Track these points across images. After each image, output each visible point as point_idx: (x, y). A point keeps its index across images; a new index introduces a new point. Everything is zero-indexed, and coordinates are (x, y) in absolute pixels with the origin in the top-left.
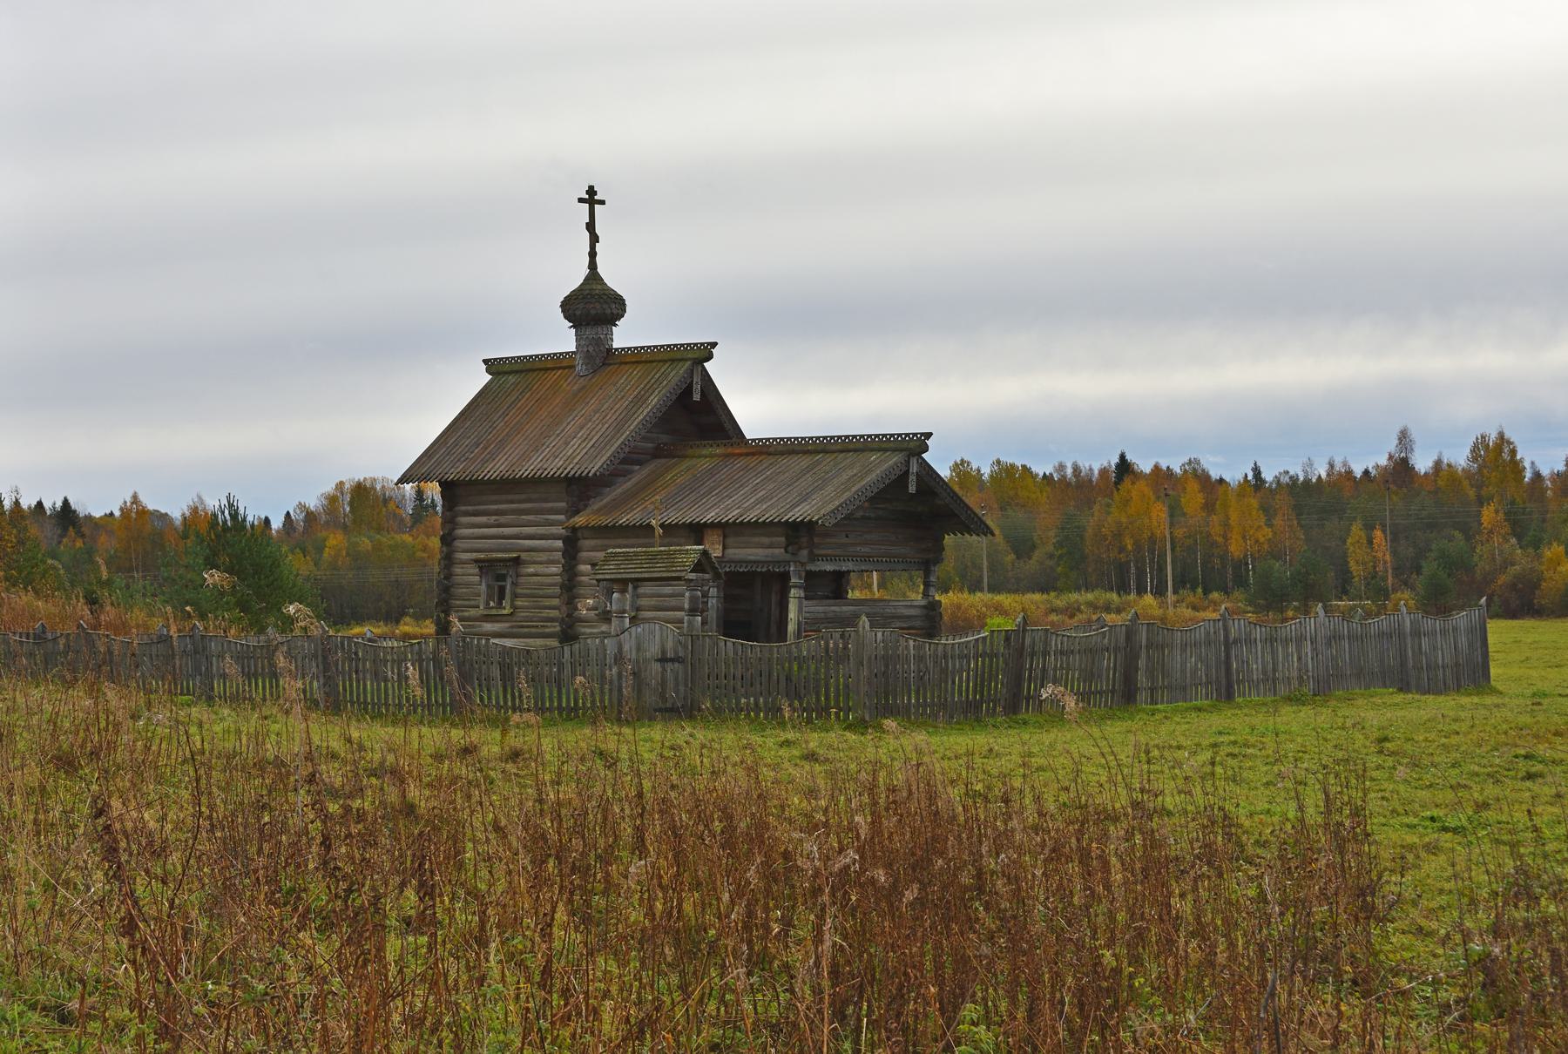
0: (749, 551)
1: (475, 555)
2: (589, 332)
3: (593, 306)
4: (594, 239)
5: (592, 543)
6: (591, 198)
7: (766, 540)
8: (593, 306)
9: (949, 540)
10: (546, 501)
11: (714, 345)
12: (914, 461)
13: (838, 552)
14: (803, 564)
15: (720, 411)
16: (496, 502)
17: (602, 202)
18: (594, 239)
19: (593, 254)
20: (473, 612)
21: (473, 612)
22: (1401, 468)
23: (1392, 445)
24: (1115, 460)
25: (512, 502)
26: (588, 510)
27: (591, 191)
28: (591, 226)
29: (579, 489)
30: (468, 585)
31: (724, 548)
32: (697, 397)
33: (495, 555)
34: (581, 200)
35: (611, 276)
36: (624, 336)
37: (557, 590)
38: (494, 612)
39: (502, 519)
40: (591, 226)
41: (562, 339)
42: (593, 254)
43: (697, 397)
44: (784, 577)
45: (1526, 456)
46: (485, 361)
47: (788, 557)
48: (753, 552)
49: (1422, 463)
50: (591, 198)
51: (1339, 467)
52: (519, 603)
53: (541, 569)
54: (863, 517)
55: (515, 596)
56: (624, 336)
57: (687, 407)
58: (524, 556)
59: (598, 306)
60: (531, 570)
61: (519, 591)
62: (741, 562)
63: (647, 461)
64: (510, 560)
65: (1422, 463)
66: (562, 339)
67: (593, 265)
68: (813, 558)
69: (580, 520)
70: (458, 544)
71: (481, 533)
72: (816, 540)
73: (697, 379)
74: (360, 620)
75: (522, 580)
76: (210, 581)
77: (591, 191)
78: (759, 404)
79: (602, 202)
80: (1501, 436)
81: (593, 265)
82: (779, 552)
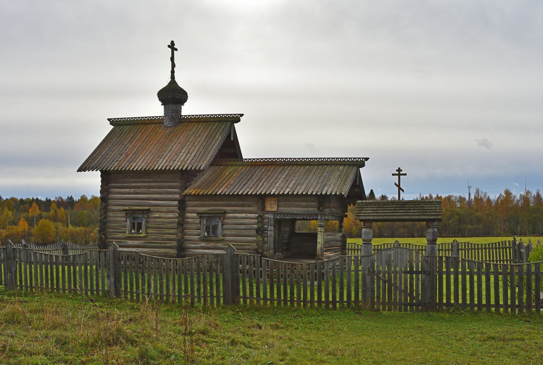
0: (293, 209)
1: (121, 208)
2: (173, 107)
3: (173, 96)
4: (173, 65)
5: (192, 203)
6: (172, 46)
7: (304, 204)
8: (173, 96)
10: (166, 182)
15: (237, 147)
16: (134, 182)
18: (173, 65)
19: (173, 72)
20: (121, 235)
21: (121, 235)
25: (144, 182)
26: (191, 187)
27: (172, 42)
28: (172, 59)
29: (186, 176)
30: (116, 222)
31: (278, 207)
32: (232, 139)
33: (134, 208)
35: (181, 82)
36: (187, 110)
37: (175, 225)
38: (135, 235)
39: (138, 190)
40: (172, 59)
41: (157, 110)
42: (173, 72)
43: (232, 139)
45: (75, 199)
46: (109, 120)
50: (172, 46)
51: (48, 198)
52: (150, 231)
53: (163, 215)
55: (147, 228)
56: (187, 110)
58: (152, 208)
59: (179, 95)
60: (157, 215)
61: (149, 225)
62: (287, 214)
64: (146, 210)
66: (157, 110)
67: (173, 77)
69: (190, 191)
70: (110, 202)
71: (126, 196)
75: (150, 220)
80: (71, 196)
81: (173, 77)
82: (316, 209)
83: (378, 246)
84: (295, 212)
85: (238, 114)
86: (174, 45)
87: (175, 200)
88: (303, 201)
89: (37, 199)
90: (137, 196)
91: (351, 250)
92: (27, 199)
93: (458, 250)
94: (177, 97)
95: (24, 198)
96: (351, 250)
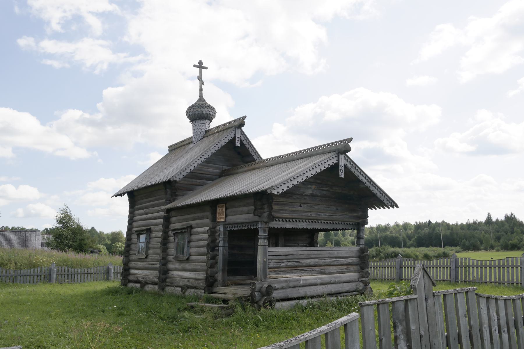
9: (371, 212)
12: (342, 157)
13: (294, 216)
14: (266, 223)
17: (206, 68)
18: (202, 83)
19: (201, 90)
22: (489, 221)
23: (487, 216)
24: (428, 221)
27: (200, 63)
31: (226, 216)
32: (238, 144)
34: (195, 66)
35: (209, 100)
37: (204, 250)
39: (147, 210)
42: (201, 90)
44: (256, 231)
47: (256, 218)
48: (242, 217)
49: (494, 220)
50: (200, 66)
54: (312, 195)
57: (236, 153)
59: (199, 110)
63: (216, 179)
65: (494, 220)
67: (201, 96)
68: (272, 218)
72: (275, 207)
74: (475, 248)
77: (200, 63)
78: (267, 144)
79: (206, 68)
81: (201, 96)
83: (499, 260)
84: (239, 221)
85: (346, 140)
86: (202, 64)
87: (159, 218)
88: (244, 206)
89: (46, 229)
91: (477, 267)
92: (100, 232)
93: (457, 267)
94: (197, 113)
95: (98, 230)
96: (477, 267)
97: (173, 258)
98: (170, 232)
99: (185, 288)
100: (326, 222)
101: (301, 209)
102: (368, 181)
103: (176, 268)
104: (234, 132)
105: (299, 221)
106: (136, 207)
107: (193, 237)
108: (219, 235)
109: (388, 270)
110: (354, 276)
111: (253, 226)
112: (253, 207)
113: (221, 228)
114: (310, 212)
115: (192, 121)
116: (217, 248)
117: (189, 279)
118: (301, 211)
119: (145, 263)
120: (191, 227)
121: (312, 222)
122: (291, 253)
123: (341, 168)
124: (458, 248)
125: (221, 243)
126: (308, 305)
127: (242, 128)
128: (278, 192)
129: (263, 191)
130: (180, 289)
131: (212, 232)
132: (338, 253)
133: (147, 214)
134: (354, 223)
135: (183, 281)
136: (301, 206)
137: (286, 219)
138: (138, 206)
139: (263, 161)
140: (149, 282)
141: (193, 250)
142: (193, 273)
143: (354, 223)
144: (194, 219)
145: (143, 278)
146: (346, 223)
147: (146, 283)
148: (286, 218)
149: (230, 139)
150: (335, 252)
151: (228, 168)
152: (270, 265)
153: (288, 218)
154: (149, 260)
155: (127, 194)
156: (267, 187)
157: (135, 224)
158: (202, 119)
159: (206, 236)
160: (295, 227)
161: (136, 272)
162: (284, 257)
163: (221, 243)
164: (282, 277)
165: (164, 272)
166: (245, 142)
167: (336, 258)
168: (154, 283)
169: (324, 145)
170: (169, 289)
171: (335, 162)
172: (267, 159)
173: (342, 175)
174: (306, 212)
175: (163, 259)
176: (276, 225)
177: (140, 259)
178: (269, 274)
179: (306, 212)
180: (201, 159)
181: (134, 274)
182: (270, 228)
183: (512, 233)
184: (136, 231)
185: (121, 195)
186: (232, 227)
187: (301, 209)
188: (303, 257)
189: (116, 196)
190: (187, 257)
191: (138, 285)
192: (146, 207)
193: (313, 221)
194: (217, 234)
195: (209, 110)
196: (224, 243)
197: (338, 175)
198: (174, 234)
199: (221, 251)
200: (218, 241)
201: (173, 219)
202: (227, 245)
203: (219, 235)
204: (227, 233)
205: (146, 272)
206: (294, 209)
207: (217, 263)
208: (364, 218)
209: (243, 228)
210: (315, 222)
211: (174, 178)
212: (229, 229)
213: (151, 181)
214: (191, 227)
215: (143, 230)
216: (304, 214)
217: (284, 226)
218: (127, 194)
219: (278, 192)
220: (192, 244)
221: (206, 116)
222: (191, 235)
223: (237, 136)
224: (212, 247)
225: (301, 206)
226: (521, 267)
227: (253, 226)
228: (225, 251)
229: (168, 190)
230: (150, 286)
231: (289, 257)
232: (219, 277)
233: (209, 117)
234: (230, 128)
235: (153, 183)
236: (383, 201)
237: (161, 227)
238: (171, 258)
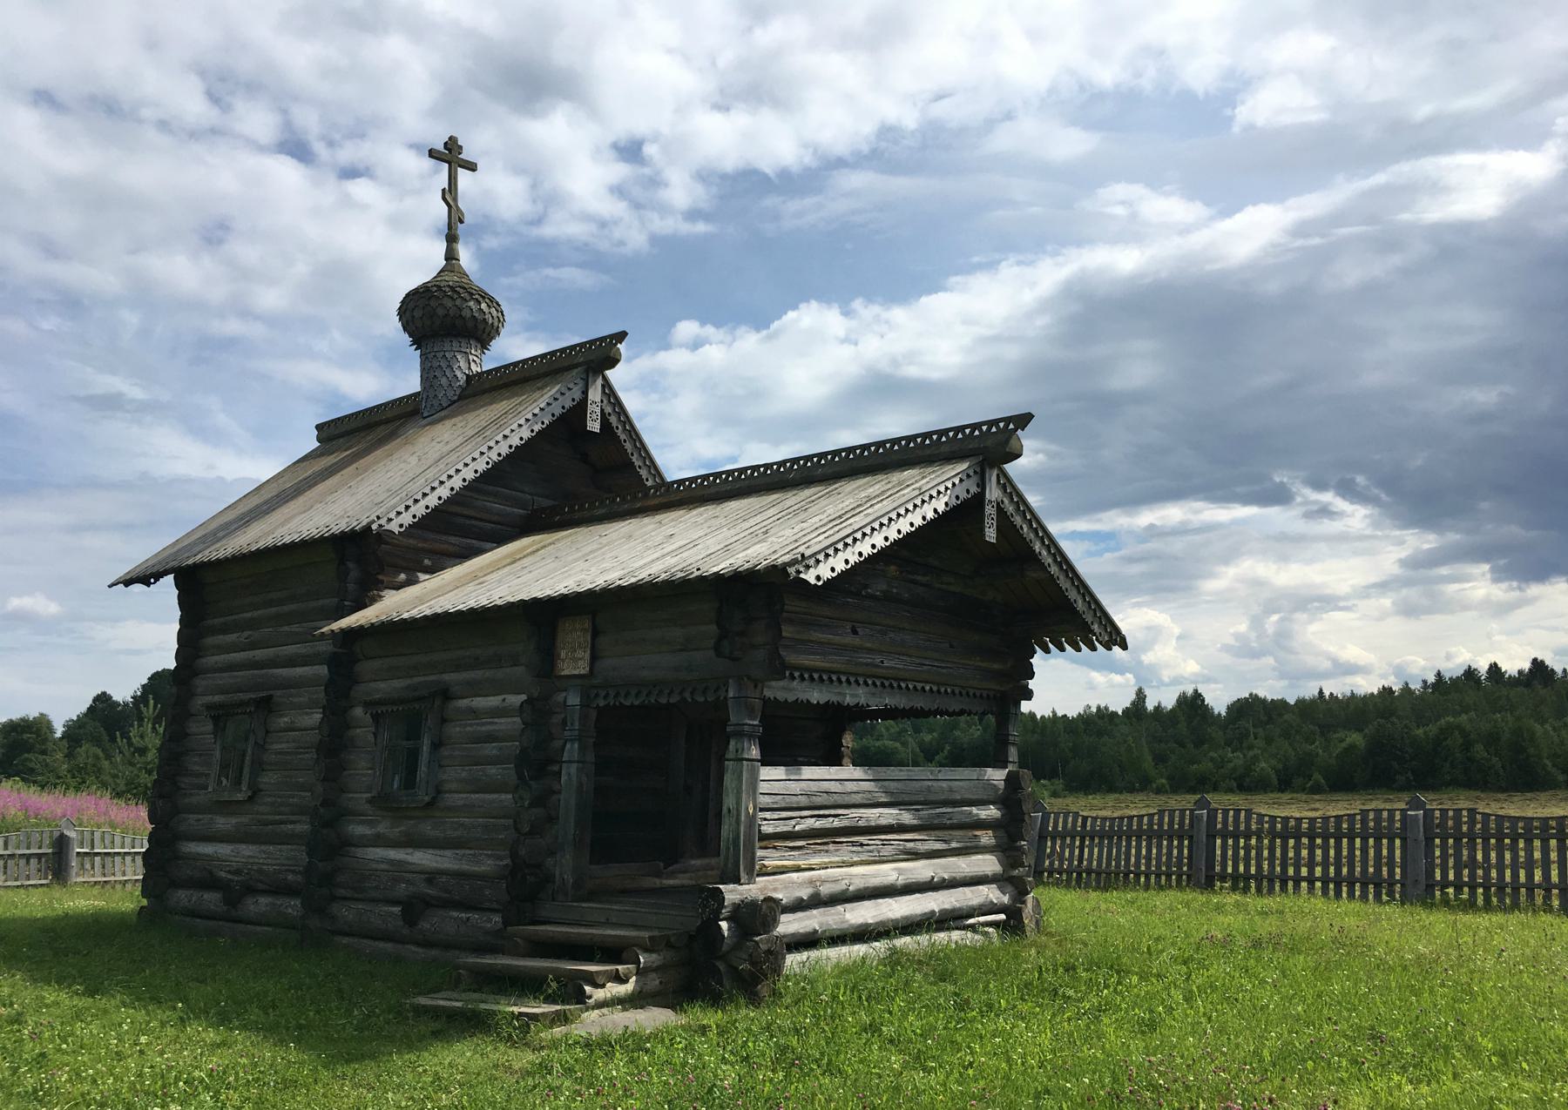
11: (621, 336)
17: (472, 167)
27: (452, 146)
31: (594, 658)
32: (594, 426)
43: (594, 426)
48: (651, 661)
49: (1150, 705)
68: (781, 670)
72: (787, 631)
73: (595, 394)
76: (767, 772)
77: (452, 146)
85: (1008, 420)
90: (259, 654)
97: (370, 801)
98: (358, 711)
99: (413, 909)
100: (919, 686)
101: (856, 641)
102: (1055, 560)
103: (378, 836)
104: (581, 384)
105: (848, 682)
106: (210, 622)
107: (454, 730)
108: (564, 722)
109: (1159, 847)
110: (988, 864)
111: (704, 692)
112: (714, 627)
113: (574, 700)
114: (880, 652)
115: (418, 342)
116: (556, 768)
117: (431, 876)
118: (856, 649)
119: (245, 819)
120: (446, 695)
121: (883, 685)
122: (826, 786)
123: (990, 511)
124: (1059, 784)
125: (572, 750)
126: (895, 959)
127: (608, 373)
128: (818, 578)
129: (773, 568)
130: (397, 909)
131: (538, 712)
132: (951, 790)
133: (253, 646)
134: (992, 694)
135: (408, 882)
136: (855, 632)
137: (813, 675)
138: (217, 621)
139: (664, 486)
140: (261, 886)
141: (453, 774)
142: (448, 853)
143: (992, 694)
144: (458, 668)
145: (238, 872)
146: (971, 692)
147: (250, 890)
148: (811, 670)
149: (569, 404)
150: (944, 784)
151: (547, 503)
152: (768, 829)
153: (816, 671)
154: (262, 809)
155: (170, 578)
156: (786, 558)
157: (200, 683)
158: (456, 336)
159: (513, 723)
160: (835, 699)
161: (207, 849)
162: (803, 801)
163: (572, 750)
164: (798, 869)
165: (329, 846)
166: (613, 420)
167: (945, 803)
168: (279, 889)
169: (808, 458)
170: (346, 913)
171: (974, 489)
172: (681, 482)
173: (991, 535)
174: (870, 651)
175: (325, 803)
176: (778, 690)
177: (225, 807)
178: (763, 858)
179: (870, 651)
180: (473, 466)
181: (197, 857)
182: (766, 701)
183: (1199, 743)
184: (209, 707)
185: (146, 577)
186: (617, 695)
187: (856, 641)
188: (857, 799)
189: (128, 582)
190: (427, 799)
191: (211, 899)
192: (252, 625)
193: (887, 683)
194: (556, 719)
195: (483, 306)
196: (582, 749)
197: (982, 530)
198: (376, 718)
199: (572, 774)
200: (557, 744)
201: (366, 667)
202: (591, 757)
203: (564, 722)
204: (593, 714)
205: (248, 850)
206: (837, 639)
207: (552, 819)
208: (1018, 682)
209: (663, 701)
210: (891, 686)
211: (383, 521)
212: (602, 703)
213: (278, 533)
214: (446, 695)
215: (242, 704)
216: (865, 658)
217: (803, 696)
218: (170, 578)
219: (818, 578)
220: (445, 752)
221: (470, 324)
222: (444, 721)
223: (590, 397)
224: (536, 764)
225: (855, 632)
226: (1191, 838)
227: (704, 692)
228: (584, 779)
229: (351, 565)
230: (264, 900)
231: (818, 800)
232: (564, 866)
233: (482, 333)
234: (569, 368)
235: (296, 537)
236: (1082, 623)
237: (320, 694)
238: (359, 799)
